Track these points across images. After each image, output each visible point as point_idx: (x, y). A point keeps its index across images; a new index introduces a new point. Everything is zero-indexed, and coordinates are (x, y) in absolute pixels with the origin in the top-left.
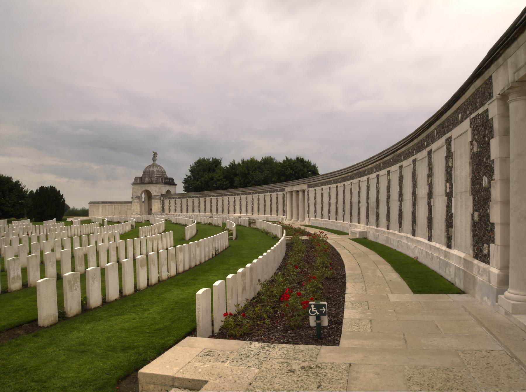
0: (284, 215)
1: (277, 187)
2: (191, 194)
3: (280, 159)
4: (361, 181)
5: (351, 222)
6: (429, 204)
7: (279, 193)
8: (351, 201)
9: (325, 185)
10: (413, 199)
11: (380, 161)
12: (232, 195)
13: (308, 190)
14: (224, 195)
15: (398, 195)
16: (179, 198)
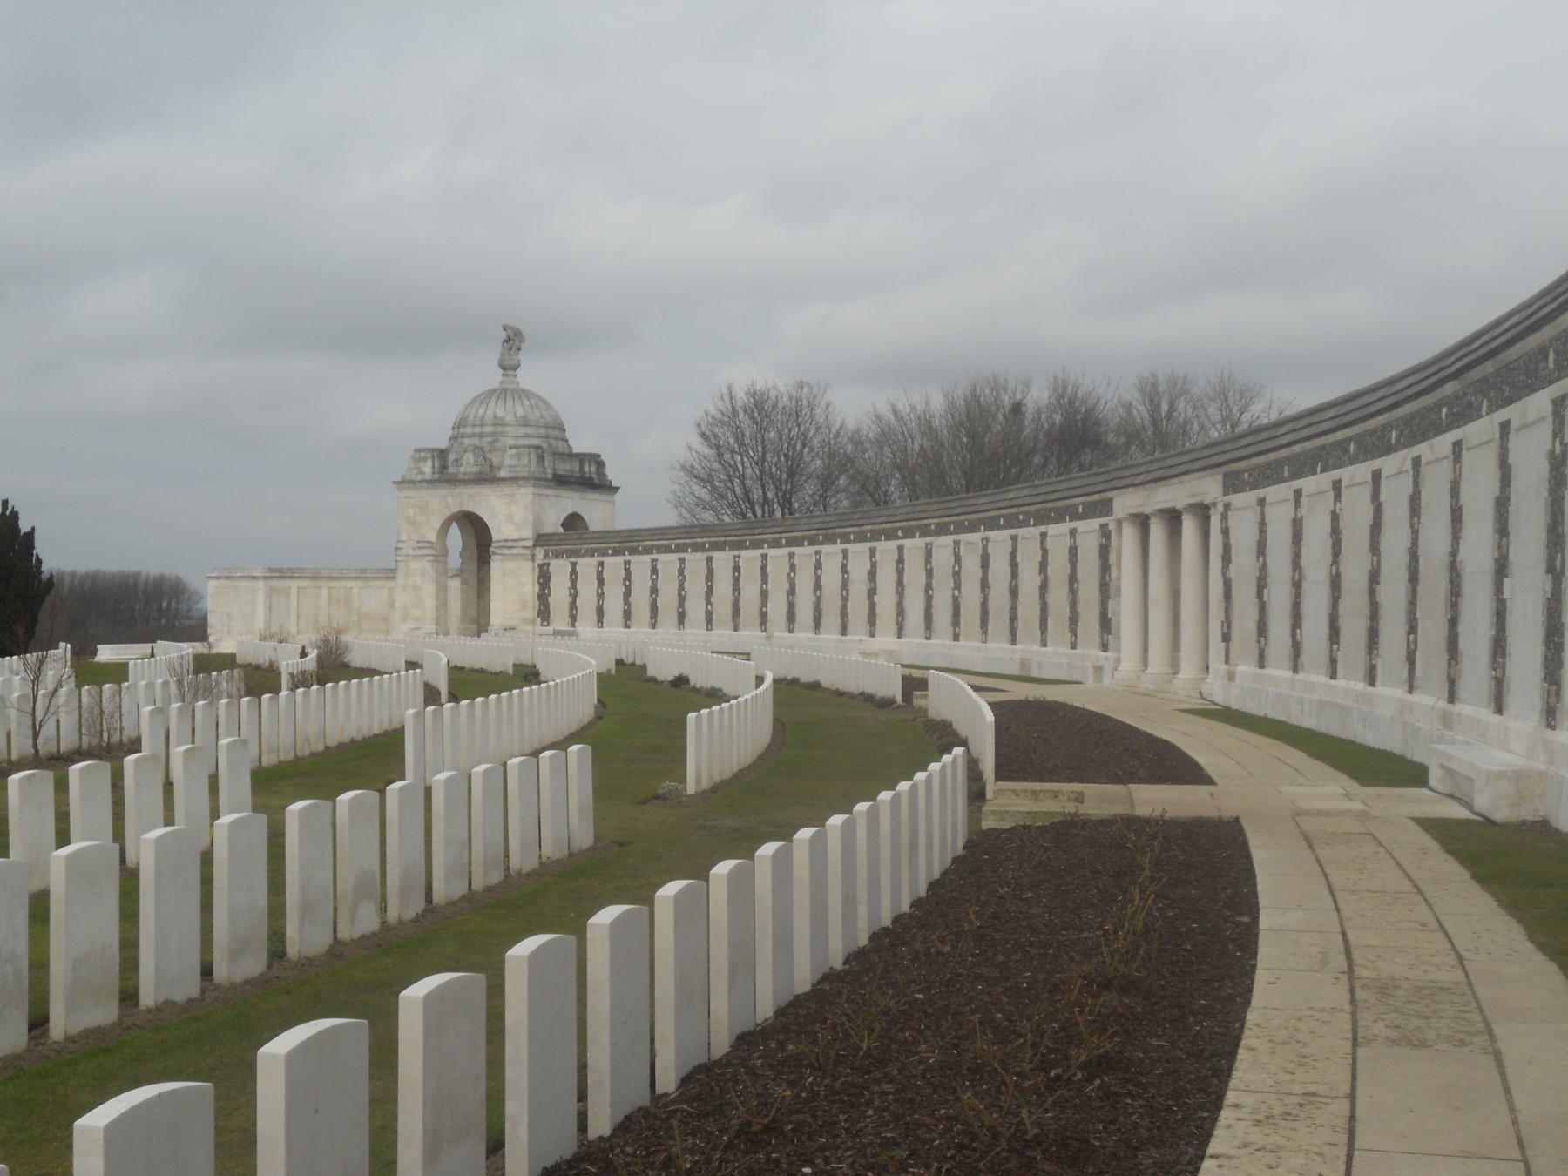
0: (1105, 648)
1: (1072, 493)
4: (1514, 425)
5: (1452, 699)
7: (1080, 525)
9: (1314, 473)
12: (861, 538)
13: (1227, 506)
14: (825, 536)
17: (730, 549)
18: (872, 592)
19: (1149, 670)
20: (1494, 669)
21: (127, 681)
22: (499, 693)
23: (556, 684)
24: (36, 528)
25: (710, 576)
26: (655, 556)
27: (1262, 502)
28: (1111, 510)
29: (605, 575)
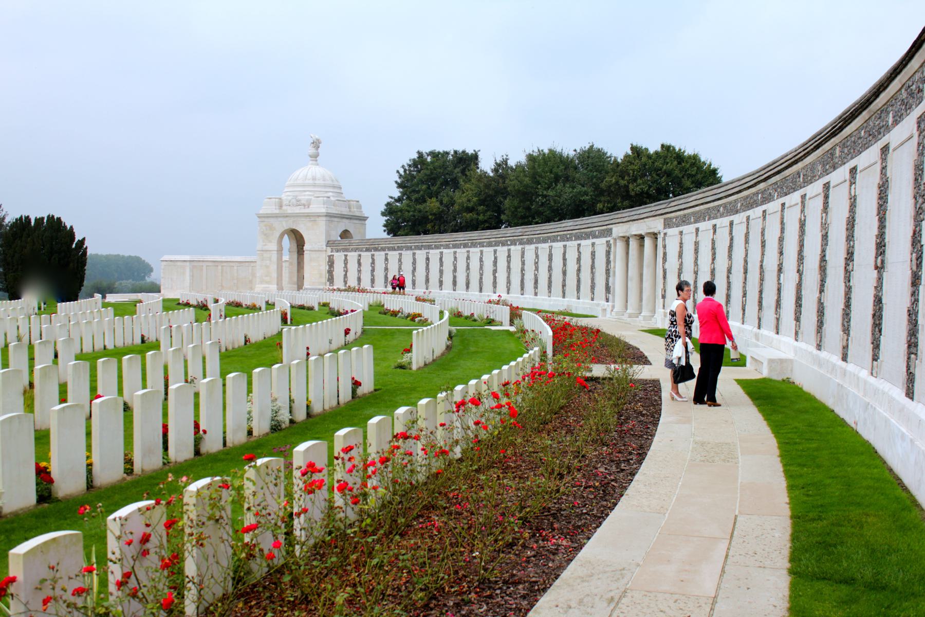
2: (399, 240)
3: (618, 151)
4: (787, 205)
5: (759, 327)
7: (597, 241)
8: (761, 266)
9: (705, 220)
10: (914, 262)
11: (833, 140)
12: (490, 245)
13: (665, 234)
14: (472, 243)
15: (873, 246)
16: (368, 250)
17: (424, 249)
18: (495, 271)
19: (628, 311)
20: (776, 314)
21: (136, 314)
22: (311, 323)
23: (423, 330)
24: (86, 239)
25: (414, 263)
26: (387, 252)
27: (681, 233)
28: (611, 234)
29: (362, 261)
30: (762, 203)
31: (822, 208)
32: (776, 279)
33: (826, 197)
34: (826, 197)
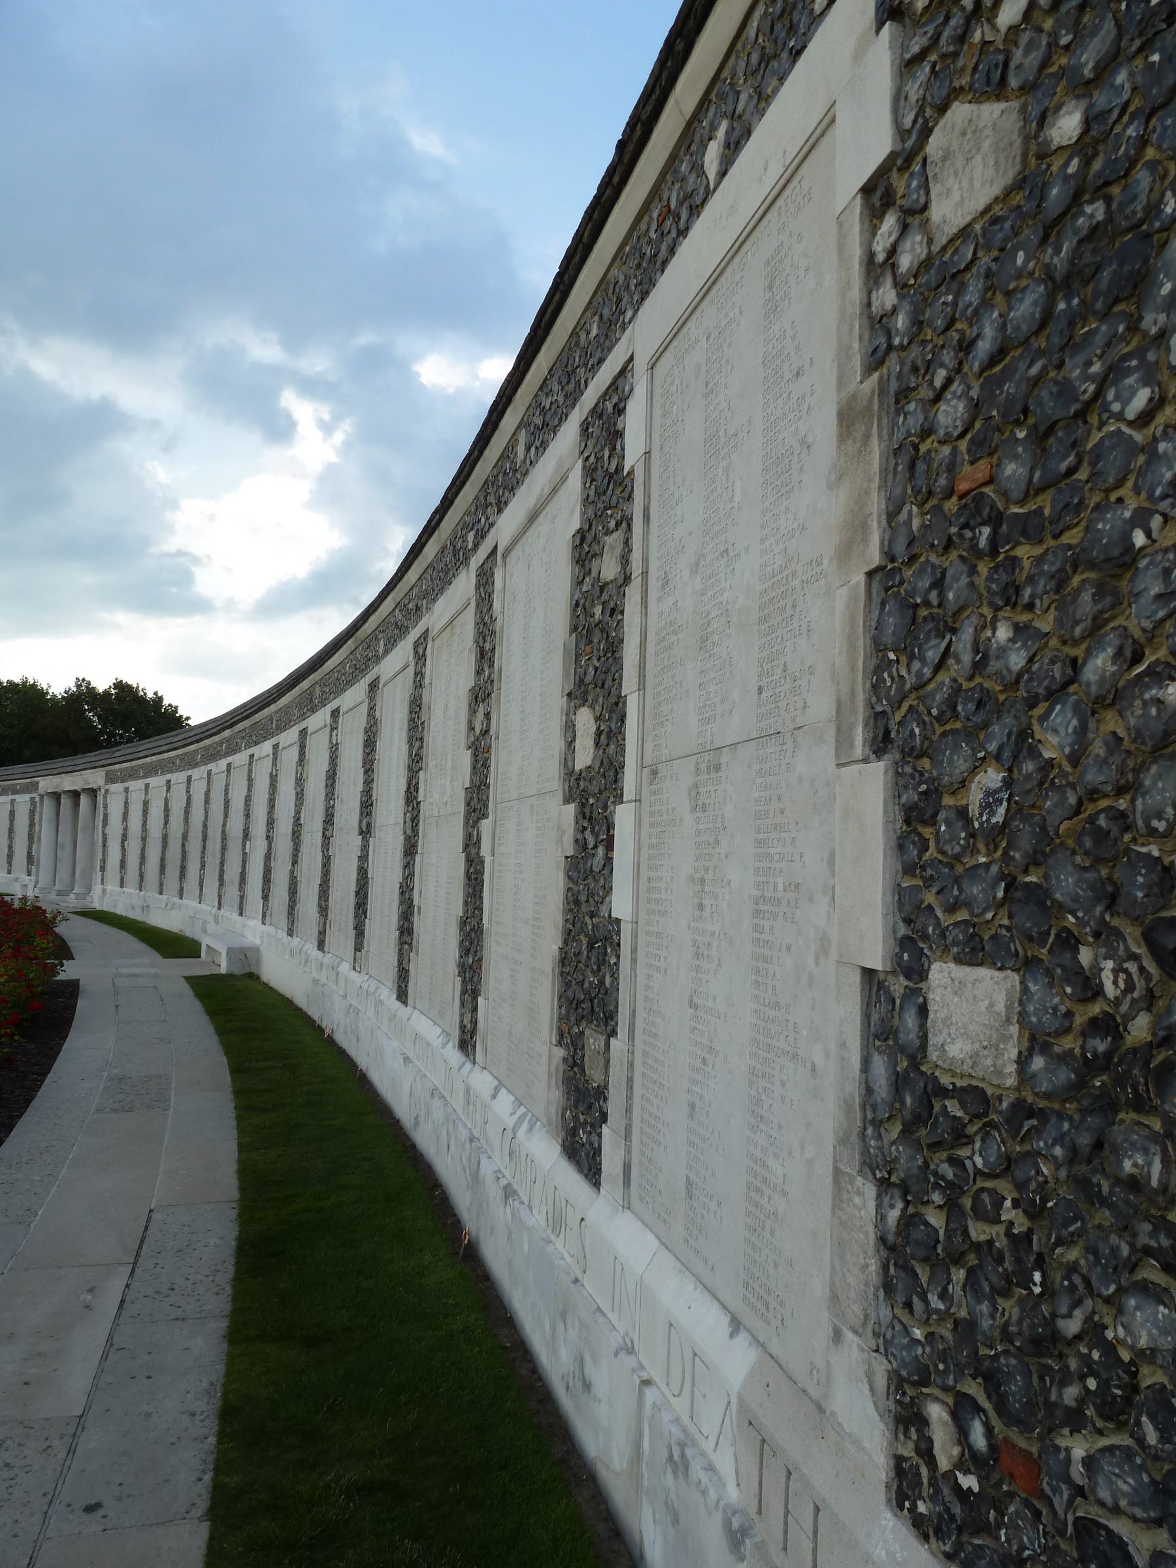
0: (29, 874)
5: (219, 908)
6: (471, 844)
7: (18, 798)
8: (224, 831)
13: (107, 791)
30: (227, 754)
31: (297, 760)
32: (240, 848)
33: (302, 747)
34: (302, 747)
